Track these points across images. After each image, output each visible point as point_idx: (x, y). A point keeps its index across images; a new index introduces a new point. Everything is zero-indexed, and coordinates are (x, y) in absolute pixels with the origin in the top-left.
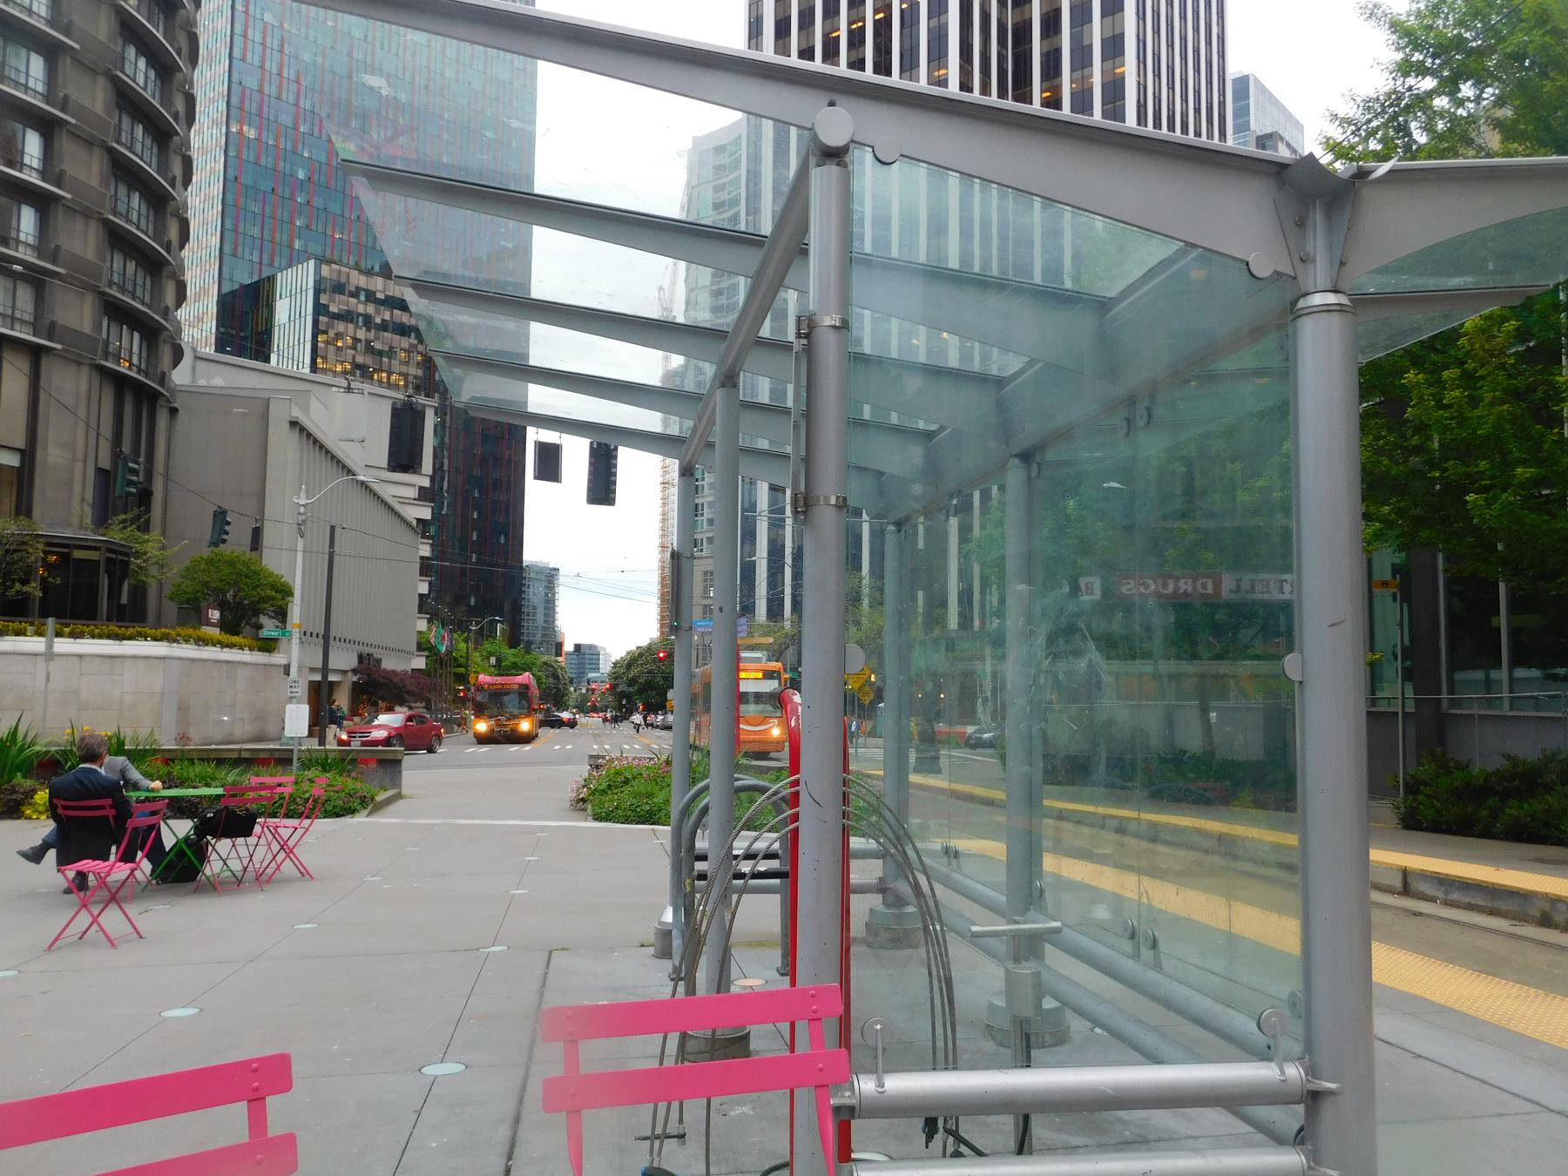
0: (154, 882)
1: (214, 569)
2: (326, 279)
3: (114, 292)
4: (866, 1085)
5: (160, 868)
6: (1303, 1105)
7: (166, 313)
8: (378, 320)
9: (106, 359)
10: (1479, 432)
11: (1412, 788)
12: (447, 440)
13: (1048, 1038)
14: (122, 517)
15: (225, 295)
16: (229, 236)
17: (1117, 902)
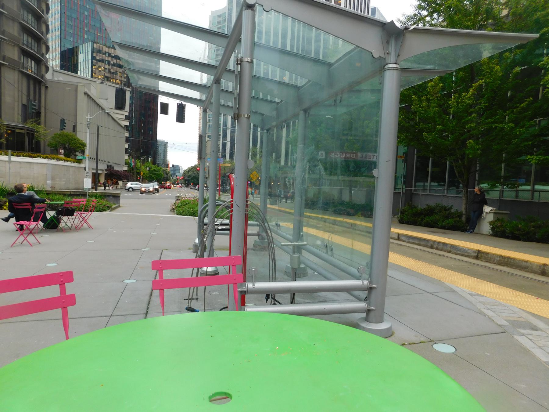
0: (44, 228)
1: (62, 138)
2: (95, 48)
3: (25, 47)
4: (250, 285)
5: (46, 224)
6: (367, 291)
7: (43, 55)
8: (112, 63)
9: (23, 69)
10: (429, 115)
11: (402, 213)
12: (134, 101)
13: (302, 275)
14: (32, 120)
15: (62, 51)
16: (63, 32)
17: (323, 240)
